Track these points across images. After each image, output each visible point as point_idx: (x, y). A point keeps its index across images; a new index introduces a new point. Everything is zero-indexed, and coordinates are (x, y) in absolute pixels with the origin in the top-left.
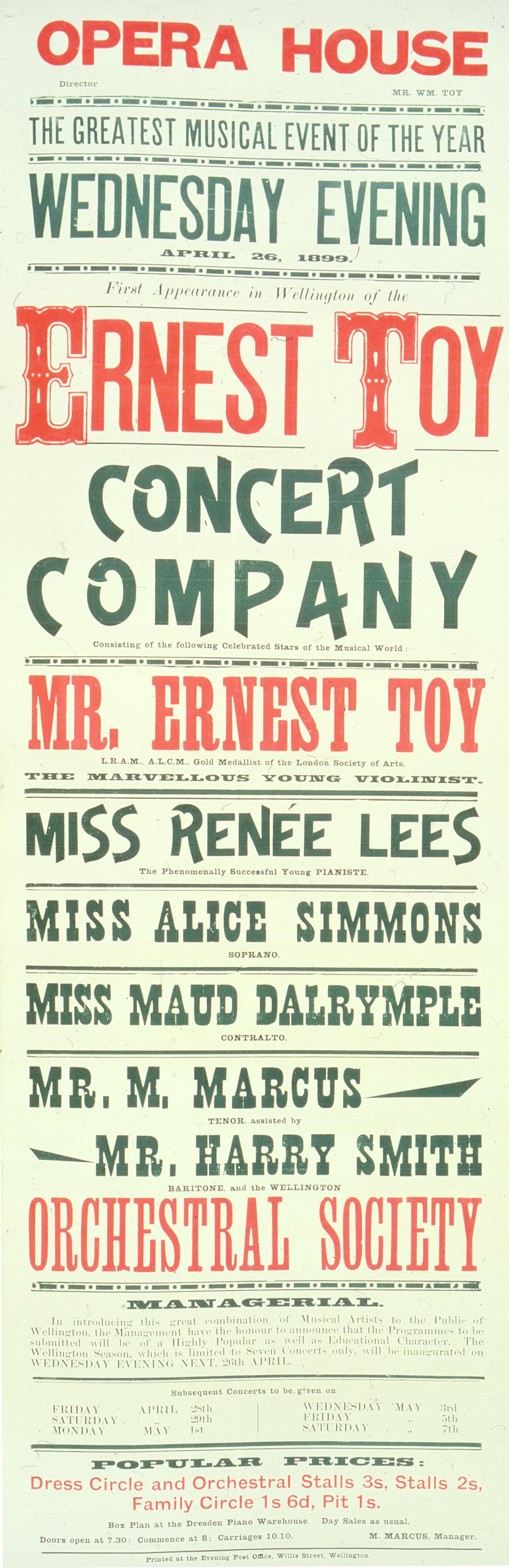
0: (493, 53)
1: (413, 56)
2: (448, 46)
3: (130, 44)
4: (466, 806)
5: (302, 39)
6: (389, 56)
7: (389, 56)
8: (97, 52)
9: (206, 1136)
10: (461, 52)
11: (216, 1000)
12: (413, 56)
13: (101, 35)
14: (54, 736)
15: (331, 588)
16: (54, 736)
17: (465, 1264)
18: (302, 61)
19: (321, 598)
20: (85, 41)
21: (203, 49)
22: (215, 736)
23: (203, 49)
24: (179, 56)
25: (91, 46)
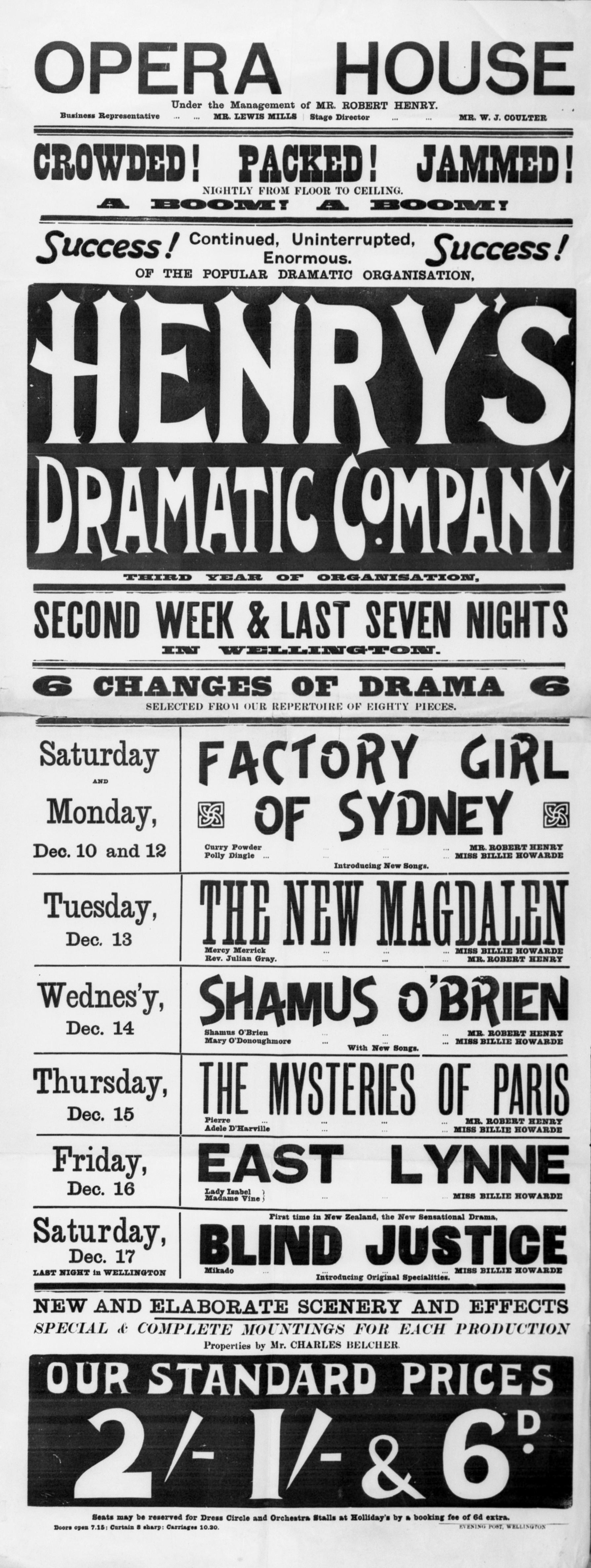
0: (576, 72)
1: (487, 71)
2: (528, 61)
3: (145, 68)
4: (213, 1027)
5: (358, 56)
6: (459, 75)
7: (459, 75)
8: (103, 77)
9: (168, 179)
10: (541, 66)
11: (126, 159)
12: (487, 71)
13: (110, 58)
14: (395, 938)
15: (248, 756)
16: (395, 938)
17: (39, 1089)
18: (357, 83)
19: (243, 762)
20: (90, 69)
21: (232, 74)
22: (282, 999)
23: (232, 74)
24: (204, 82)
25: (97, 71)
